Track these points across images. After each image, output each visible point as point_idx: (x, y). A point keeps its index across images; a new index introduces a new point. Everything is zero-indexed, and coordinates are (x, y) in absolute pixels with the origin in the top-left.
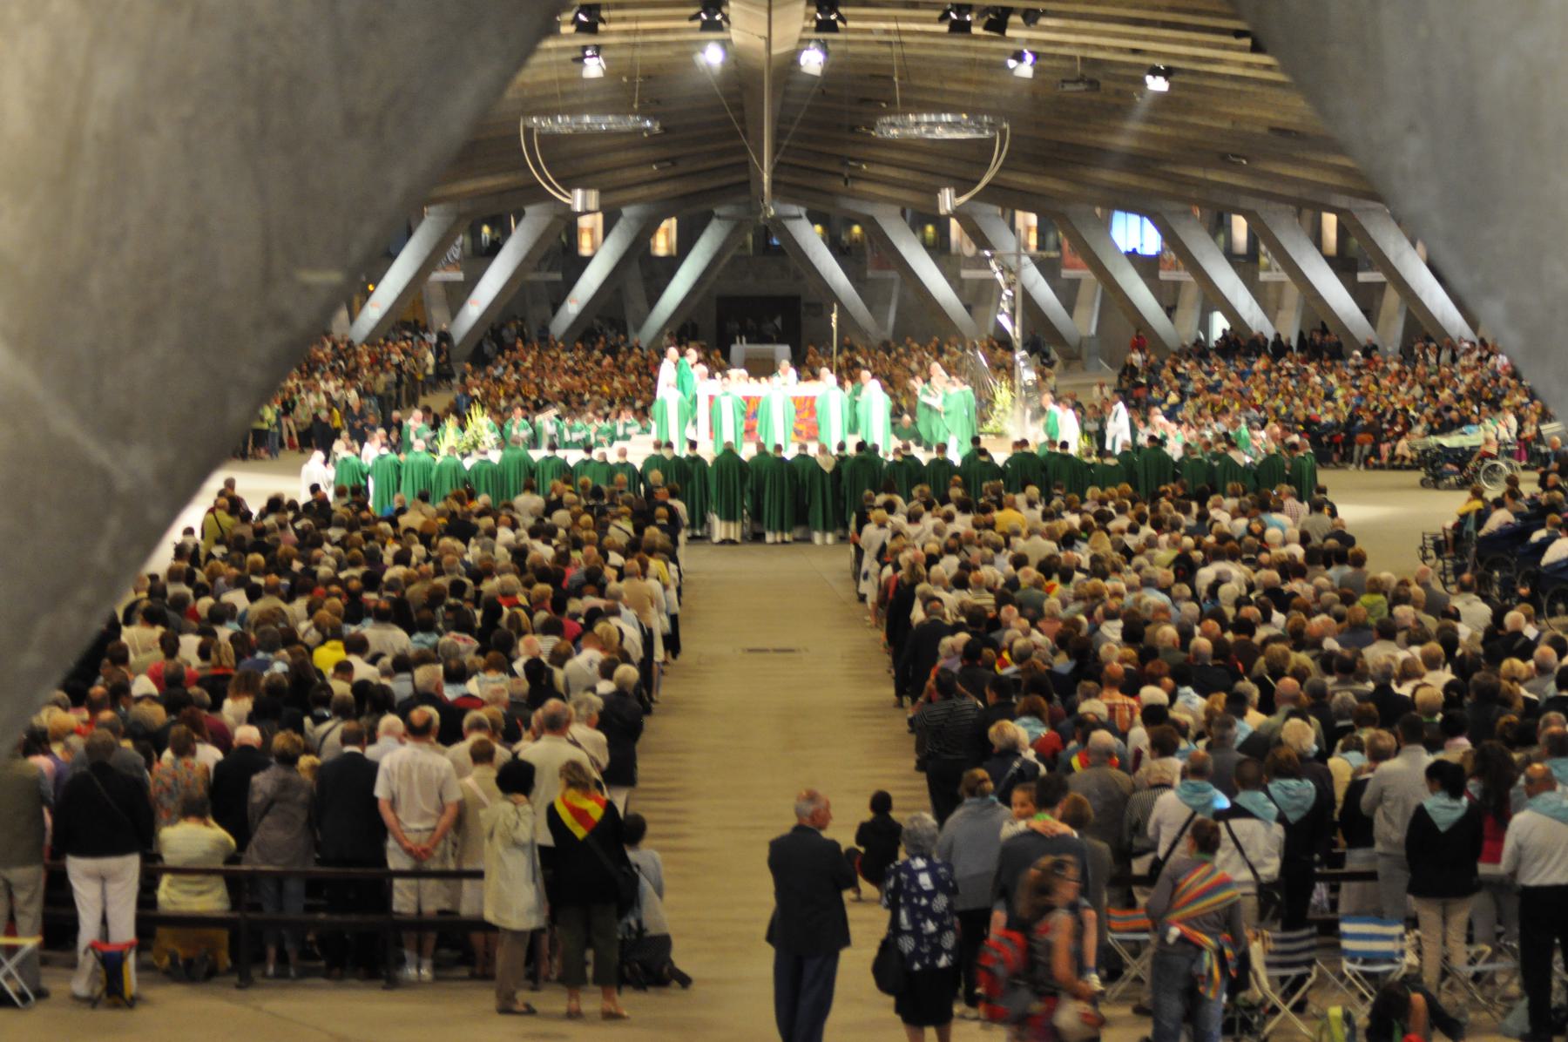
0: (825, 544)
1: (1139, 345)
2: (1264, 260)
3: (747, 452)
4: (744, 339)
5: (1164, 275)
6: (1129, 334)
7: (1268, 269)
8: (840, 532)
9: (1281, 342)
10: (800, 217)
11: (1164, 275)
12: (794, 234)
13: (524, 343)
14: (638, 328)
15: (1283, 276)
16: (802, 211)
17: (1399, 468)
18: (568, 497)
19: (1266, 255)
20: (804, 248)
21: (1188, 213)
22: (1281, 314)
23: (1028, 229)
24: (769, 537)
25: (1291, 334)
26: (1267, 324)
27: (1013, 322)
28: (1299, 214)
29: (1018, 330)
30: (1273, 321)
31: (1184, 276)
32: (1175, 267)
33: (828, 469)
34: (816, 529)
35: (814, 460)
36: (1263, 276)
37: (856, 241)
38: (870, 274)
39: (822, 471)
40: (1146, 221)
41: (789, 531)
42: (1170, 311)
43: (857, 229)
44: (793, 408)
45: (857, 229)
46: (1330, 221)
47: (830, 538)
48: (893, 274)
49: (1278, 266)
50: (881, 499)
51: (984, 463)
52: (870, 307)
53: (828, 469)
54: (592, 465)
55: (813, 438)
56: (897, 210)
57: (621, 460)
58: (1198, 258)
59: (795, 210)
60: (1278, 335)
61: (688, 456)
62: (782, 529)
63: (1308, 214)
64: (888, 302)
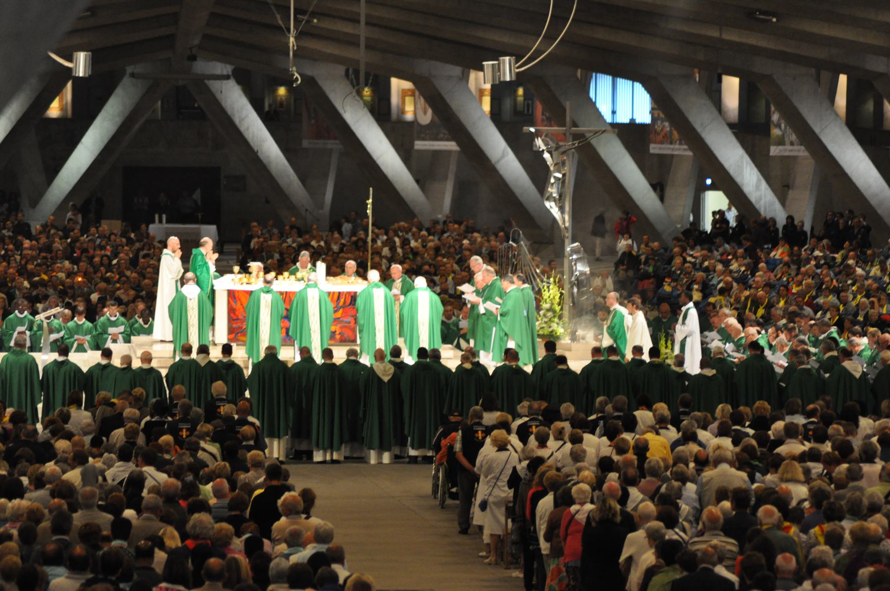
0: (380, 463)
1: (624, 230)
2: (776, 132)
3: (289, 355)
4: (164, 217)
5: (655, 149)
6: (614, 216)
7: (781, 142)
8: (397, 450)
9: (795, 227)
10: (227, 77)
11: (655, 149)
12: (218, 96)
13: (822, 284)
14: (35, 201)
15: (800, 151)
16: (227, 69)
17: (501, 339)
18: (128, 412)
19: (778, 126)
20: (229, 112)
21: (689, 77)
22: (791, 194)
23: (481, 92)
24: (318, 456)
25: (806, 219)
26: (777, 205)
27: (562, 209)
28: (818, 79)
29: (567, 217)
30: (783, 201)
31: (681, 150)
32: (668, 139)
33: (386, 379)
34: (370, 448)
35: (371, 370)
36: (774, 151)
37: (281, 104)
38: (305, 143)
39: (380, 379)
40: (638, 86)
41: (339, 449)
42: (659, 187)
43: (282, 91)
44: (331, 306)
45: (282, 91)
46: (731, 86)
47: (386, 458)
48: (334, 145)
49: (794, 137)
50: (490, 418)
51: (562, 370)
52: (303, 179)
53: (386, 379)
54: (109, 369)
55: (343, 341)
56: (340, 70)
57: (146, 366)
58: (699, 129)
59: (221, 68)
60: (790, 218)
61: (220, 361)
62: (331, 447)
63: (825, 75)
64: (326, 176)
